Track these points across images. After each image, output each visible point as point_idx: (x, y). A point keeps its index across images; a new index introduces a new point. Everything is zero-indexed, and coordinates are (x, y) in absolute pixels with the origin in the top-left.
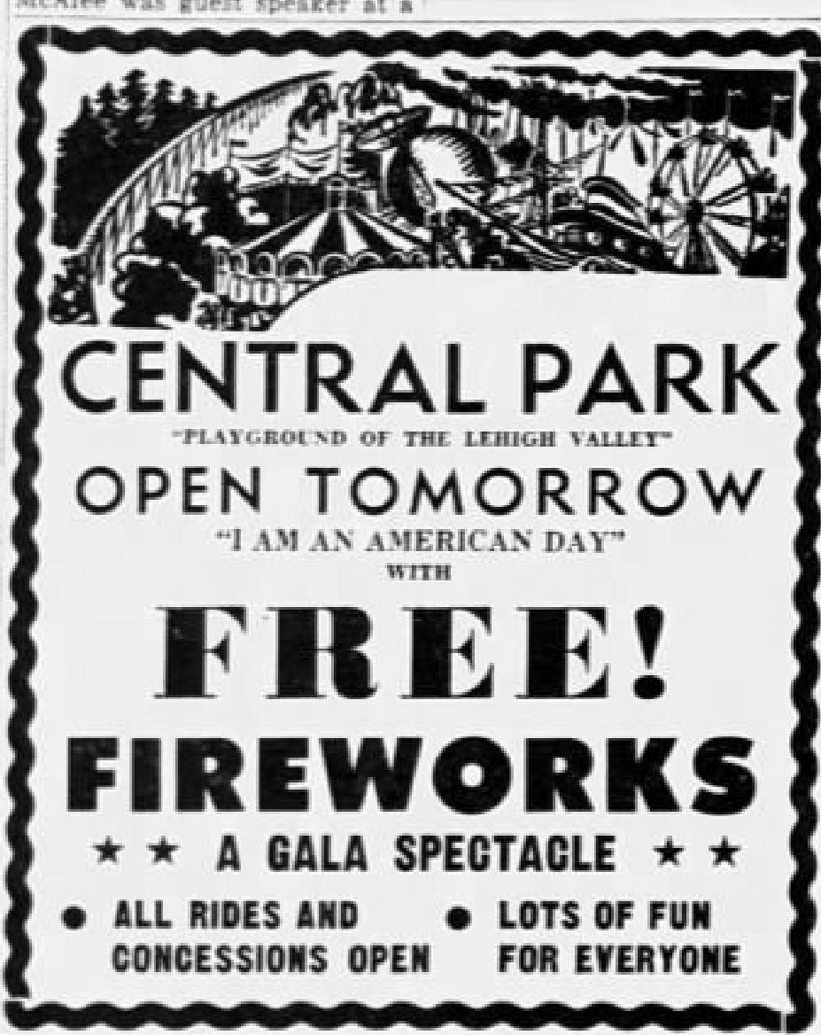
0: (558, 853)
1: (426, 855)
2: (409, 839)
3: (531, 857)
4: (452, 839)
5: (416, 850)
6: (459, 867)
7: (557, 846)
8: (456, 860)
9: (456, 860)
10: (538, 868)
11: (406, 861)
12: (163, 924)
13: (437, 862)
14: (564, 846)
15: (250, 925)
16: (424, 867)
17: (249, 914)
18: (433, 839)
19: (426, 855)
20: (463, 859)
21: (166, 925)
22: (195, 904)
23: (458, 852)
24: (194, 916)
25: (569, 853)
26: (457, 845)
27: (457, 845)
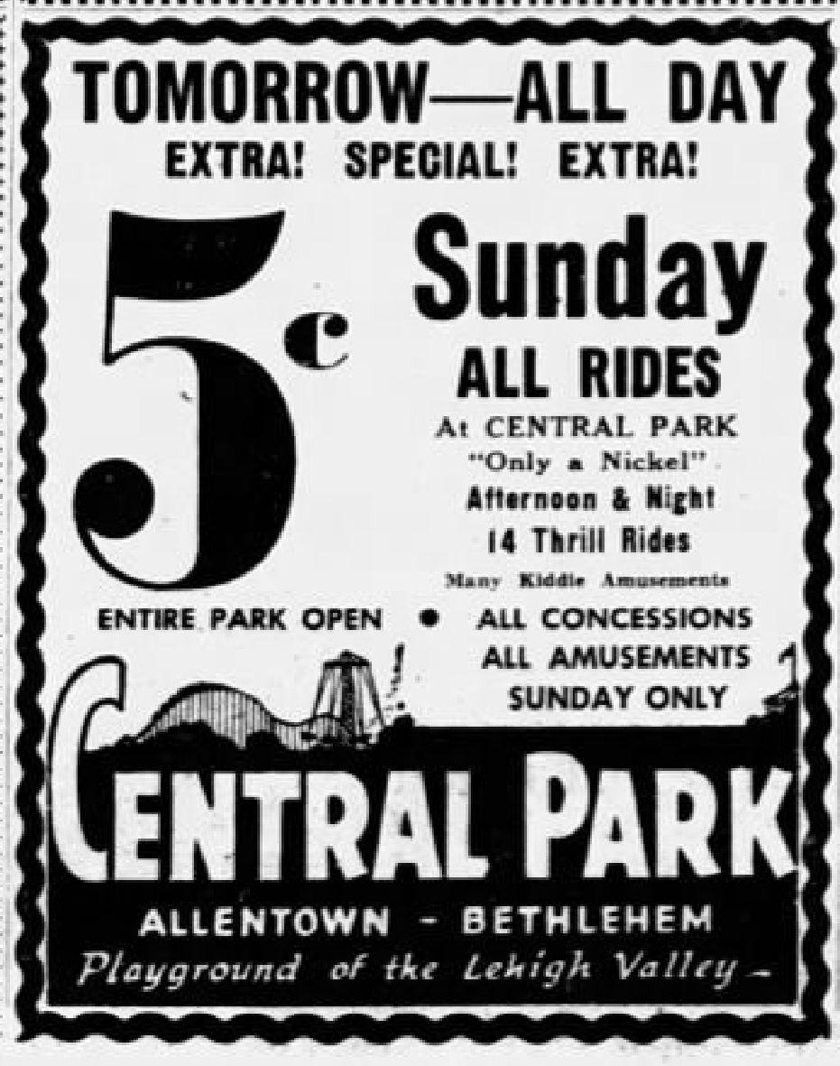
0: (430, 159)
1: (377, 162)
2: (360, 146)
3: (468, 163)
4: (402, 146)
5: (367, 157)
6: (410, 175)
7: (429, 153)
8: (408, 167)
9: (408, 167)
10: (476, 173)
11: (356, 167)
12: (534, 391)
13: (388, 169)
14: (436, 152)
15: (676, 391)
16: (375, 174)
17: (676, 370)
18: (384, 146)
19: (377, 162)
20: (413, 166)
21: (543, 393)
22: (587, 354)
23: (409, 159)
24: (587, 372)
25: (442, 159)
26: (408, 152)
27: (408, 152)
